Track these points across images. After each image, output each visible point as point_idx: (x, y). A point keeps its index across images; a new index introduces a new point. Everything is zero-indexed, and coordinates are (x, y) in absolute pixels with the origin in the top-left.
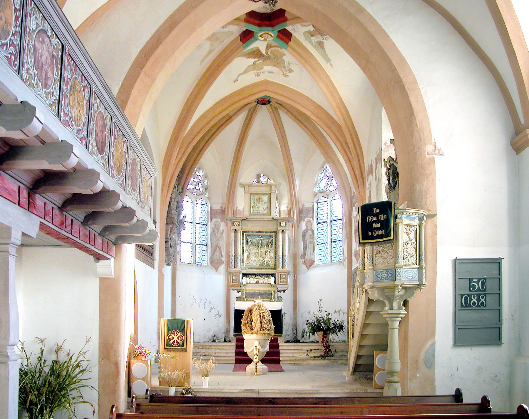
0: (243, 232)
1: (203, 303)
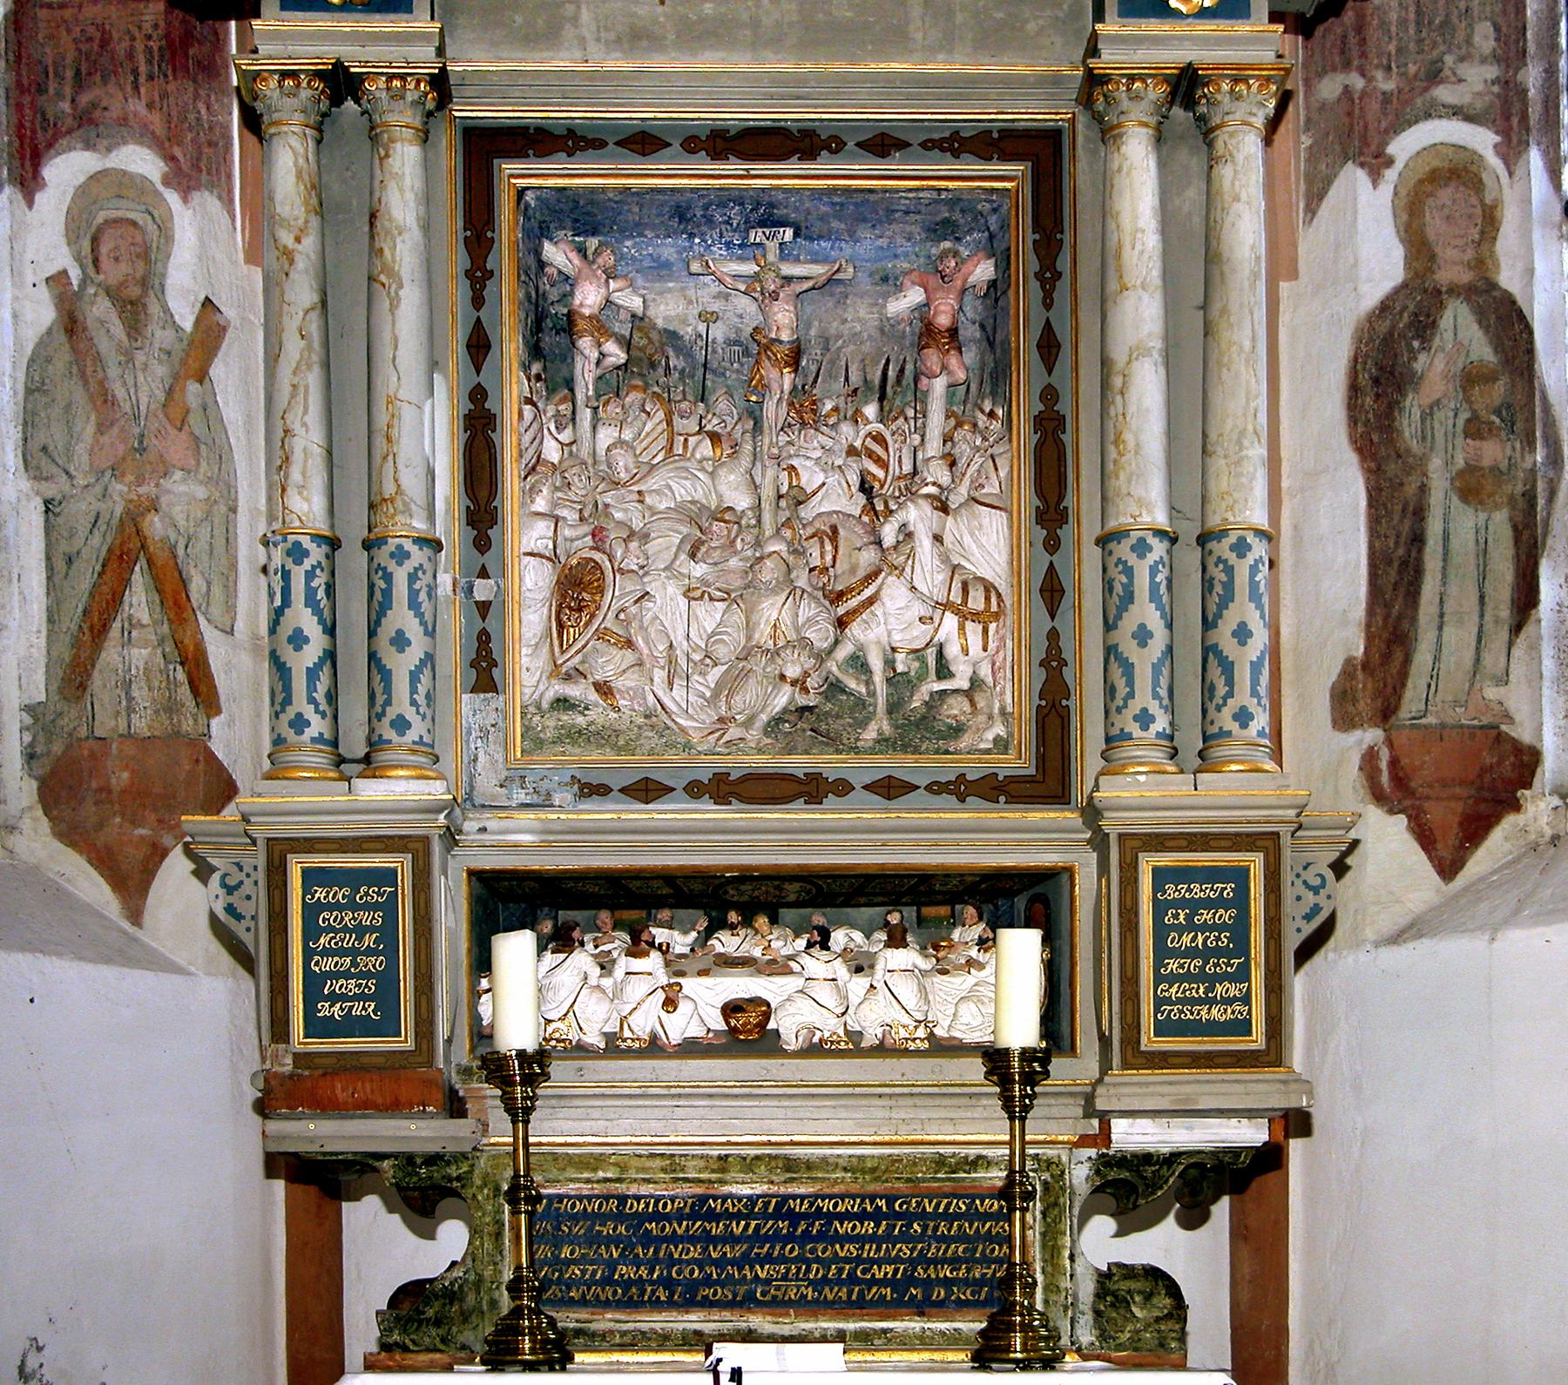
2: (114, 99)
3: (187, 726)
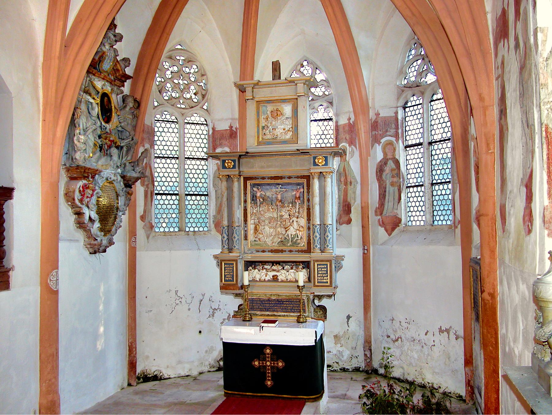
0: (246, 179)
1: (196, 302)
2: (224, 142)
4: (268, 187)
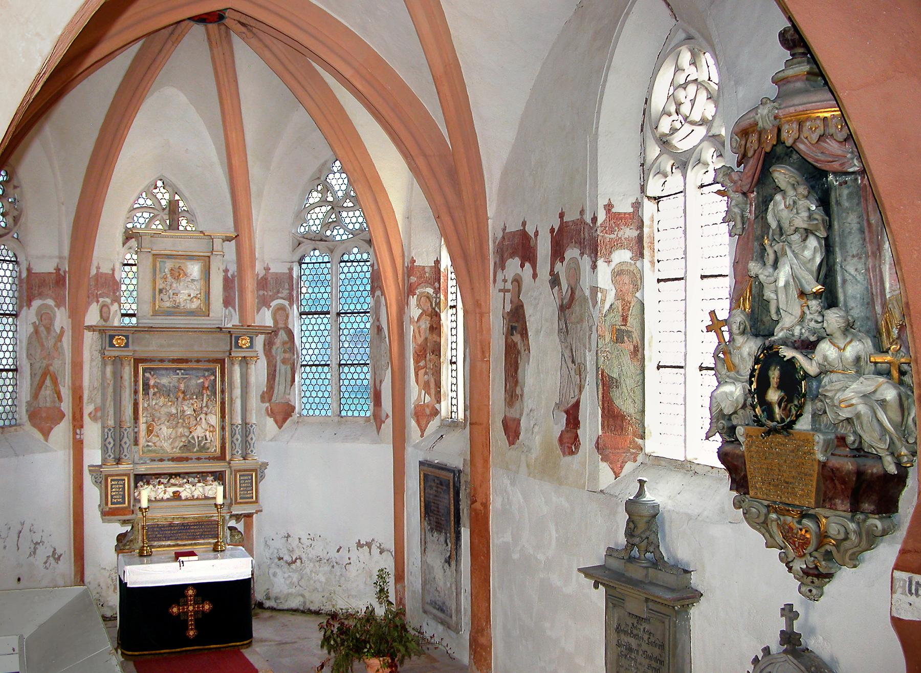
0: (137, 361)
3: (57, 405)
4: (164, 372)
